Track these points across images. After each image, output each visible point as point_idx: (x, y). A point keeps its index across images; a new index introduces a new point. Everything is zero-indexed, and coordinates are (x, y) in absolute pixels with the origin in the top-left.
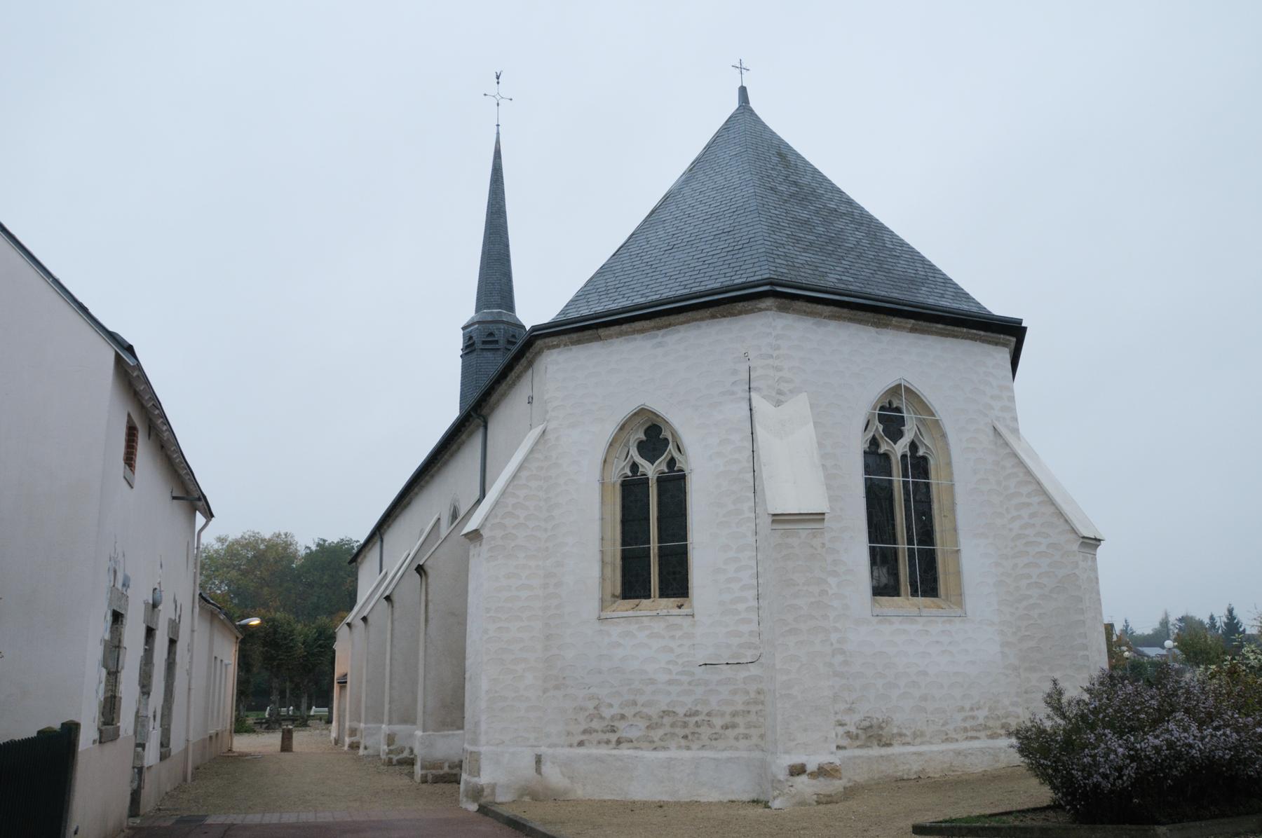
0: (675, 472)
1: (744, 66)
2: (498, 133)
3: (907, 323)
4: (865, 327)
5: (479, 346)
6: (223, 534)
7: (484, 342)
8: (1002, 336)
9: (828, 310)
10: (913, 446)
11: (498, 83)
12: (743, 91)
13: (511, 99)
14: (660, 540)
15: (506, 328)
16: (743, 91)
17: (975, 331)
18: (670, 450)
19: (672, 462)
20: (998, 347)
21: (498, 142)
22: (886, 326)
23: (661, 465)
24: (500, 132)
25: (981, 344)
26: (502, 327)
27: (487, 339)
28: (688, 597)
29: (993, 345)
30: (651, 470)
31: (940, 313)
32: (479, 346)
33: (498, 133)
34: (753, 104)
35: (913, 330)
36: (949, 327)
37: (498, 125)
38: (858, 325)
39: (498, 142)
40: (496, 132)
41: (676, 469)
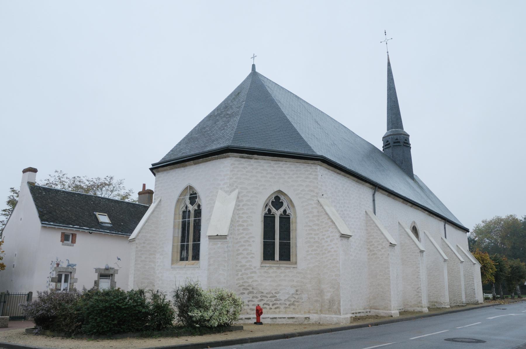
0: (271, 215)
1: (255, 58)
2: (388, 56)
3: (191, 163)
4: (181, 168)
5: (392, 144)
6: (484, 219)
7: (395, 143)
8: (224, 154)
9: (168, 167)
10: (285, 211)
11: (386, 35)
12: (254, 66)
13: (392, 39)
14: (274, 244)
15: (393, 137)
16: (254, 66)
17: (214, 156)
18: (270, 205)
19: (285, 211)
20: (227, 158)
21: (388, 60)
22: (186, 166)
23: (281, 210)
24: (389, 55)
25: (220, 160)
26: (391, 137)
27: (387, 144)
28: (199, 260)
29: (224, 158)
30: (278, 213)
31: (188, 158)
32: (392, 144)
33: (388, 56)
34: (257, 70)
35: (195, 164)
36: (204, 159)
37: (388, 52)
38: (179, 169)
39: (388, 60)
40: (387, 55)
41: (271, 214)
